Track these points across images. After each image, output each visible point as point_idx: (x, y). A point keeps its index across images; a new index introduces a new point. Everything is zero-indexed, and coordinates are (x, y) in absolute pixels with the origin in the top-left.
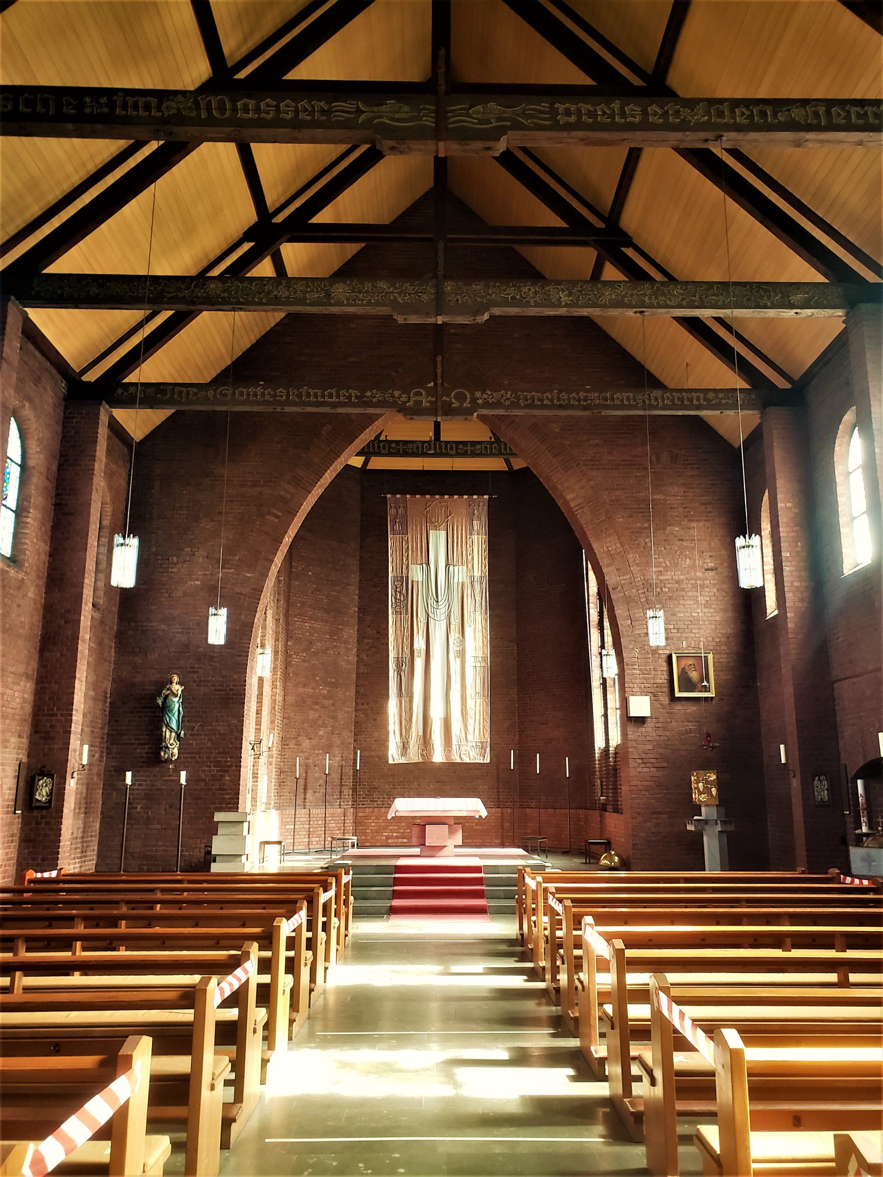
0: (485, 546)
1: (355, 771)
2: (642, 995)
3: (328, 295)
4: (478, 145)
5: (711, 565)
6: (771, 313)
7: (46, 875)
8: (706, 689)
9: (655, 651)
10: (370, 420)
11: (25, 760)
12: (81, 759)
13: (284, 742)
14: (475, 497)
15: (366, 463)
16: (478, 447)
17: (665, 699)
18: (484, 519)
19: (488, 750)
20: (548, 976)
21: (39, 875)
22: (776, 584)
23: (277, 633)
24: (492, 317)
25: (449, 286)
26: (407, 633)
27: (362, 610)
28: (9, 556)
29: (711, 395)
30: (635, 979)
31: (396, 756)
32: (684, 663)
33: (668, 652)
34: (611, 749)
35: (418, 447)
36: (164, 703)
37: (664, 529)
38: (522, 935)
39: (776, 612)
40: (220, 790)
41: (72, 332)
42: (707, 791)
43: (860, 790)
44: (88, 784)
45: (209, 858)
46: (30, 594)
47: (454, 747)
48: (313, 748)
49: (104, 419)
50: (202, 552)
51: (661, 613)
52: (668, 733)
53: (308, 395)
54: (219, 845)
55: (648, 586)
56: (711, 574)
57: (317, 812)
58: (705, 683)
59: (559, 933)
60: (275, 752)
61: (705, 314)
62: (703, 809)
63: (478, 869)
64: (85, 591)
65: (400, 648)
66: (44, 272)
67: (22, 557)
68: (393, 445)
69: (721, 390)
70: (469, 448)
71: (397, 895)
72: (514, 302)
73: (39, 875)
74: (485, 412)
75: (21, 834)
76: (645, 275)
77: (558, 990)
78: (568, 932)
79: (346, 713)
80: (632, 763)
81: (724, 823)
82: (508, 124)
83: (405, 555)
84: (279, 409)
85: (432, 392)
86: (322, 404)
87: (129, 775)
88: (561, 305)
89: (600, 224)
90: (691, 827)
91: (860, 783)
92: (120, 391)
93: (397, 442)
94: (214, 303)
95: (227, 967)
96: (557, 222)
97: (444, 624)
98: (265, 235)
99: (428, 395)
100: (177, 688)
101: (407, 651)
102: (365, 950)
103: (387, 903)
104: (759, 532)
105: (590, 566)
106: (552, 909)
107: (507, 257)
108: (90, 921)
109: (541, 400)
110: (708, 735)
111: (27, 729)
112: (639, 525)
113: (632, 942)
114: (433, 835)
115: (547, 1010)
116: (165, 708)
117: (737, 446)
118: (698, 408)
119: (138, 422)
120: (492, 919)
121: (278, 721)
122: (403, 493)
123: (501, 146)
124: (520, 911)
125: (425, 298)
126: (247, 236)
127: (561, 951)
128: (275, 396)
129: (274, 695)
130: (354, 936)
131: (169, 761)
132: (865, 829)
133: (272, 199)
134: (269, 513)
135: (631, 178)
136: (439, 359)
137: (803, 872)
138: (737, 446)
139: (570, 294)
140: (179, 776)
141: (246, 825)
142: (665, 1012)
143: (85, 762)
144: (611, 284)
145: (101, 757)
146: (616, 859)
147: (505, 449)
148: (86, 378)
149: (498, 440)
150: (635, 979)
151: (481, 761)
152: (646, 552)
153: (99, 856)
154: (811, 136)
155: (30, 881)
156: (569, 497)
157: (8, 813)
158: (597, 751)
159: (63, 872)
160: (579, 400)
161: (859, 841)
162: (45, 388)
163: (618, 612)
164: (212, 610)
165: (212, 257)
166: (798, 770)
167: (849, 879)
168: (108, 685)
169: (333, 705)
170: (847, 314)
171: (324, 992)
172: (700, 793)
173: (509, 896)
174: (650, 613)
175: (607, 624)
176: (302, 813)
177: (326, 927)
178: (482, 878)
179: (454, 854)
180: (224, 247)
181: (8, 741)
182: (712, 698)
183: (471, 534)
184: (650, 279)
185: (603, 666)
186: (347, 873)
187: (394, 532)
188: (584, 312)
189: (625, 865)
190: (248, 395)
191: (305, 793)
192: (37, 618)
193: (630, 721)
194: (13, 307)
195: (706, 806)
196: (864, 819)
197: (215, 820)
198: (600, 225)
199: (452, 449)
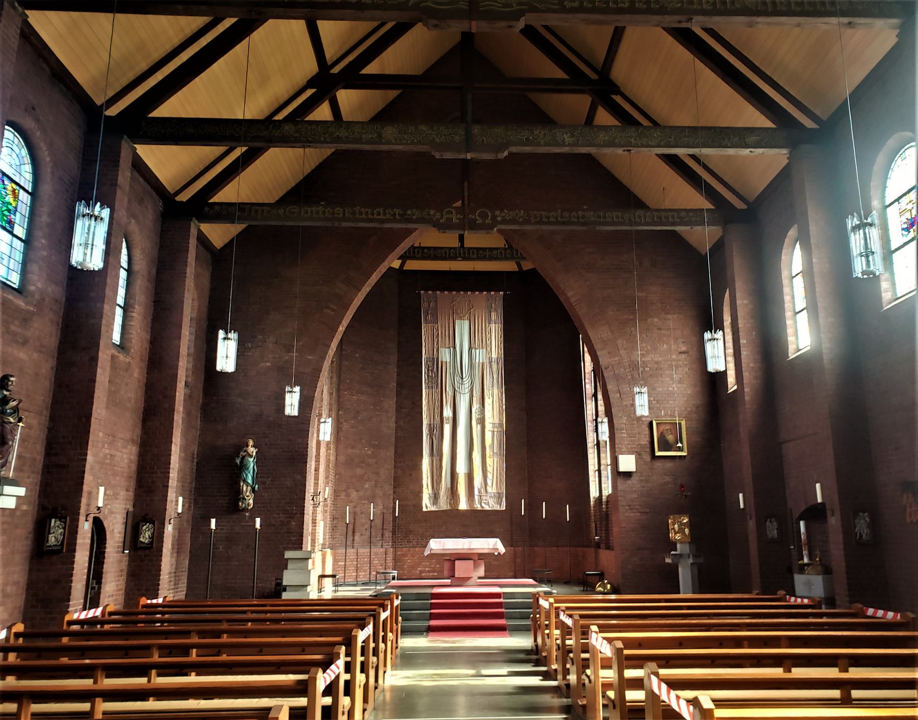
0: (501, 333)
1: (394, 517)
2: (637, 684)
3: (380, 136)
4: (503, 24)
5: (684, 349)
6: (731, 151)
7: (154, 601)
8: (680, 449)
9: (640, 418)
10: (409, 232)
11: (131, 509)
12: (177, 509)
13: (336, 493)
14: (492, 293)
15: (402, 265)
16: (495, 252)
17: (648, 458)
18: (500, 311)
19: (504, 499)
20: (560, 677)
21: (149, 602)
22: (735, 365)
23: (330, 404)
24: (510, 154)
25: (476, 129)
26: (438, 404)
27: (400, 385)
28: (118, 343)
29: (683, 214)
30: (629, 673)
31: (429, 505)
32: (662, 428)
33: (649, 419)
34: (604, 498)
35: (446, 253)
36: (242, 462)
37: (646, 320)
38: (537, 646)
39: (735, 387)
40: (289, 533)
41: (168, 162)
42: (681, 531)
43: (803, 529)
44: (179, 529)
45: (280, 588)
46: (136, 375)
47: (476, 497)
48: (360, 498)
49: (193, 232)
50: (272, 339)
51: (645, 390)
52: (650, 485)
53: (361, 213)
54: (288, 578)
55: (634, 366)
56: (683, 356)
57: (364, 551)
58: (679, 445)
59: (568, 642)
60: (329, 502)
61: (680, 152)
62: (678, 546)
63: (498, 595)
64: (179, 372)
65: (432, 417)
66: (150, 116)
67: (128, 345)
68: (426, 251)
69: (691, 210)
70: (487, 253)
71: (433, 617)
72: (528, 143)
73: (149, 602)
74: (503, 227)
75: (128, 570)
76: (634, 121)
77: (568, 686)
78: (577, 641)
79: (387, 471)
80: (621, 509)
81: (695, 556)
82: (526, 7)
83: (436, 340)
84: (336, 224)
85: (460, 211)
86: (371, 220)
87: (213, 521)
88: (564, 144)
89: (594, 76)
90: (668, 560)
91: (802, 523)
92: (207, 209)
93: (429, 248)
94: (285, 141)
95: (325, 665)
96: (560, 74)
97: (467, 397)
98: (324, 83)
99: (457, 214)
100: (252, 450)
101: (438, 419)
102: (408, 659)
103: (426, 624)
104: (722, 329)
105: (586, 349)
106: (563, 623)
107: (520, 105)
108: (202, 634)
109: (548, 218)
110: (682, 486)
111: (133, 484)
112: (626, 317)
113: (628, 643)
114: (461, 568)
115: (557, 701)
116: (243, 467)
117: (704, 254)
118: (673, 224)
119: (219, 234)
120: (511, 636)
121: (331, 477)
122: (434, 290)
123: (521, 24)
124: (535, 629)
125: (457, 138)
126: (310, 84)
127: (571, 655)
128: (333, 213)
129: (328, 455)
130: (402, 648)
131: (245, 510)
132: (806, 560)
133: (330, 53)
134: (328, 308)
135: (620, 41)
136: (466, 184)
137: (758, 594)
138: (704, 254)
139: (572, 136)
140: (255, 522)
141: (310, 561)
142: (656, 691)
143: (180, 511)
144: (605, 128)
145: (190, 506)
146: (609, 586)
147: (517, 253)
148: (179, 198)
149: (510, 247)
150: (629, 673)
151: (498, 509)
152: (632, 340)
153: (188, 588)
154: (760, 19)
155: (144, 606)
156: (570, 294)
157: (118, 552)
158: (592, 500)
159: (167, 599)
160: (578, 218)
161: (802, 569)
162: (147, 207)
163: (609, 387)
164: (288, 388)
165: (282, 101)
166: (754, 513)
167: (793, 599)
168: (195, 448)
169: (376, 463)
170: (790, 153)
171: (383, 690)
172: (676, 533)
173: (526, 616)
174: (637, 389)
175: (600, 396)
176: (351, 552)
177: (385, 640)
178: (501, 603)
179: (477, 584)
180: (292, 93)
181: (118, 494)
182: (685, 456)
183: (489, 323)
184: (638, 124)
185: (598, 431)
186: (397, 598)
187: (426, 322)
188: (584, 150)
189: (615, 591)
190: (312, 212)
191: (354, 536)
192: (141, 394)
193: (619, 476)
194: (125, 145)
195: (681, 543)
196: (805, 552)
197: (286, 557)
198: (594, 76)
199: (473, 253)
